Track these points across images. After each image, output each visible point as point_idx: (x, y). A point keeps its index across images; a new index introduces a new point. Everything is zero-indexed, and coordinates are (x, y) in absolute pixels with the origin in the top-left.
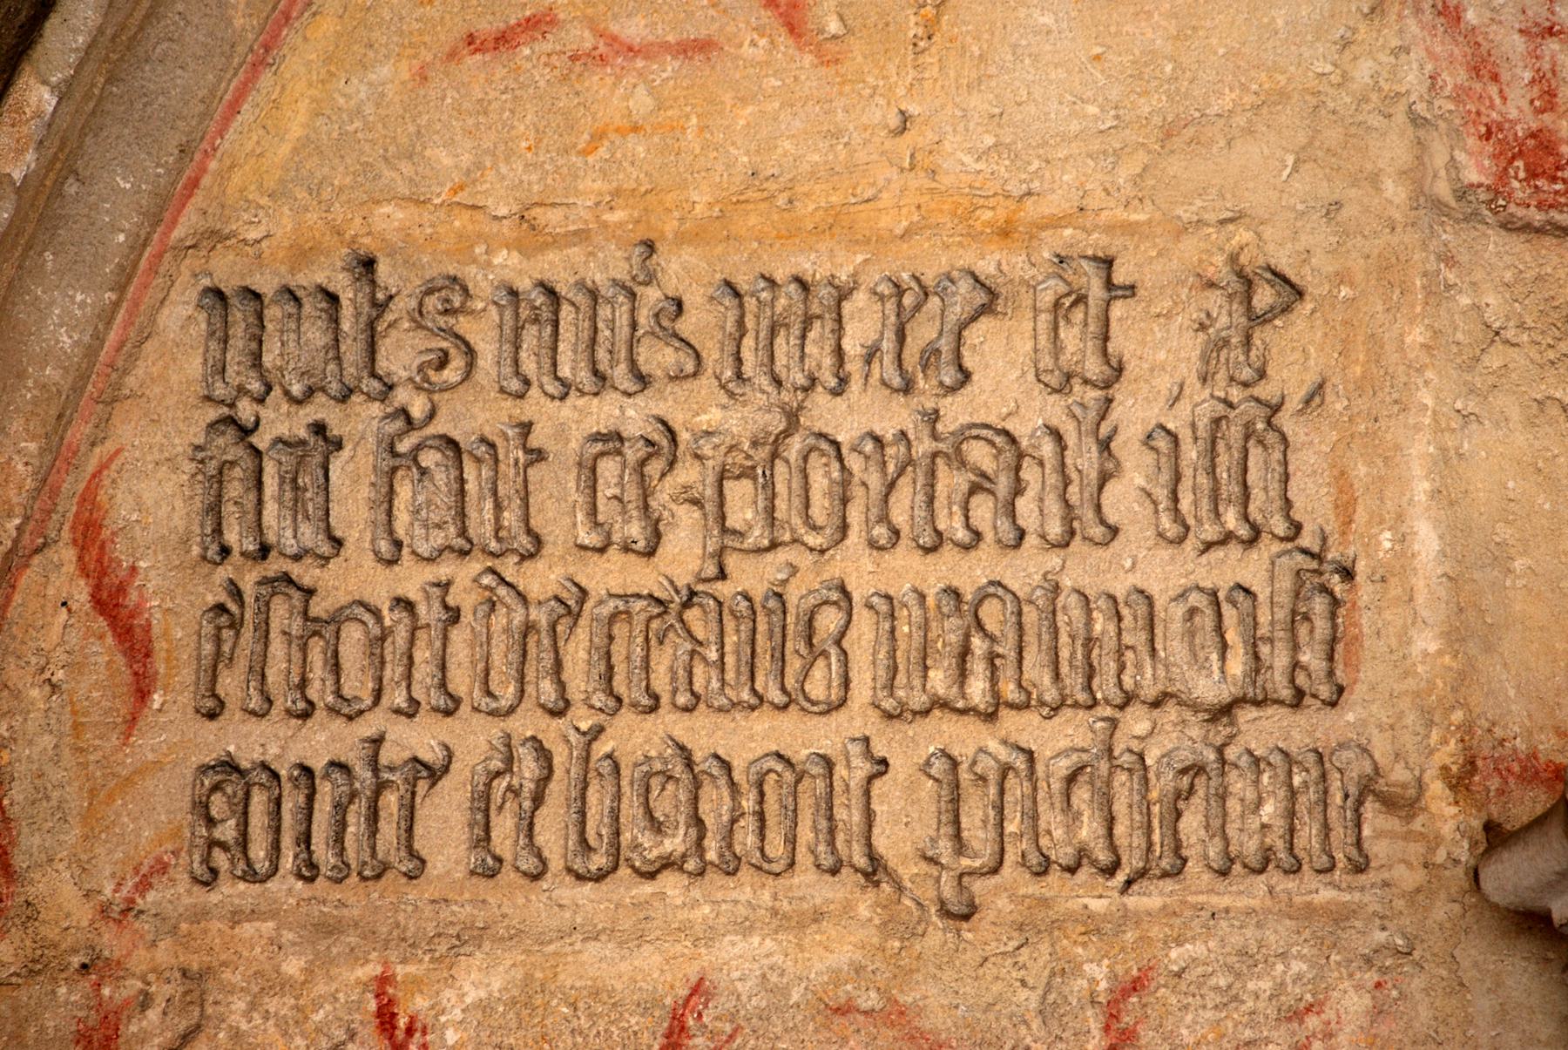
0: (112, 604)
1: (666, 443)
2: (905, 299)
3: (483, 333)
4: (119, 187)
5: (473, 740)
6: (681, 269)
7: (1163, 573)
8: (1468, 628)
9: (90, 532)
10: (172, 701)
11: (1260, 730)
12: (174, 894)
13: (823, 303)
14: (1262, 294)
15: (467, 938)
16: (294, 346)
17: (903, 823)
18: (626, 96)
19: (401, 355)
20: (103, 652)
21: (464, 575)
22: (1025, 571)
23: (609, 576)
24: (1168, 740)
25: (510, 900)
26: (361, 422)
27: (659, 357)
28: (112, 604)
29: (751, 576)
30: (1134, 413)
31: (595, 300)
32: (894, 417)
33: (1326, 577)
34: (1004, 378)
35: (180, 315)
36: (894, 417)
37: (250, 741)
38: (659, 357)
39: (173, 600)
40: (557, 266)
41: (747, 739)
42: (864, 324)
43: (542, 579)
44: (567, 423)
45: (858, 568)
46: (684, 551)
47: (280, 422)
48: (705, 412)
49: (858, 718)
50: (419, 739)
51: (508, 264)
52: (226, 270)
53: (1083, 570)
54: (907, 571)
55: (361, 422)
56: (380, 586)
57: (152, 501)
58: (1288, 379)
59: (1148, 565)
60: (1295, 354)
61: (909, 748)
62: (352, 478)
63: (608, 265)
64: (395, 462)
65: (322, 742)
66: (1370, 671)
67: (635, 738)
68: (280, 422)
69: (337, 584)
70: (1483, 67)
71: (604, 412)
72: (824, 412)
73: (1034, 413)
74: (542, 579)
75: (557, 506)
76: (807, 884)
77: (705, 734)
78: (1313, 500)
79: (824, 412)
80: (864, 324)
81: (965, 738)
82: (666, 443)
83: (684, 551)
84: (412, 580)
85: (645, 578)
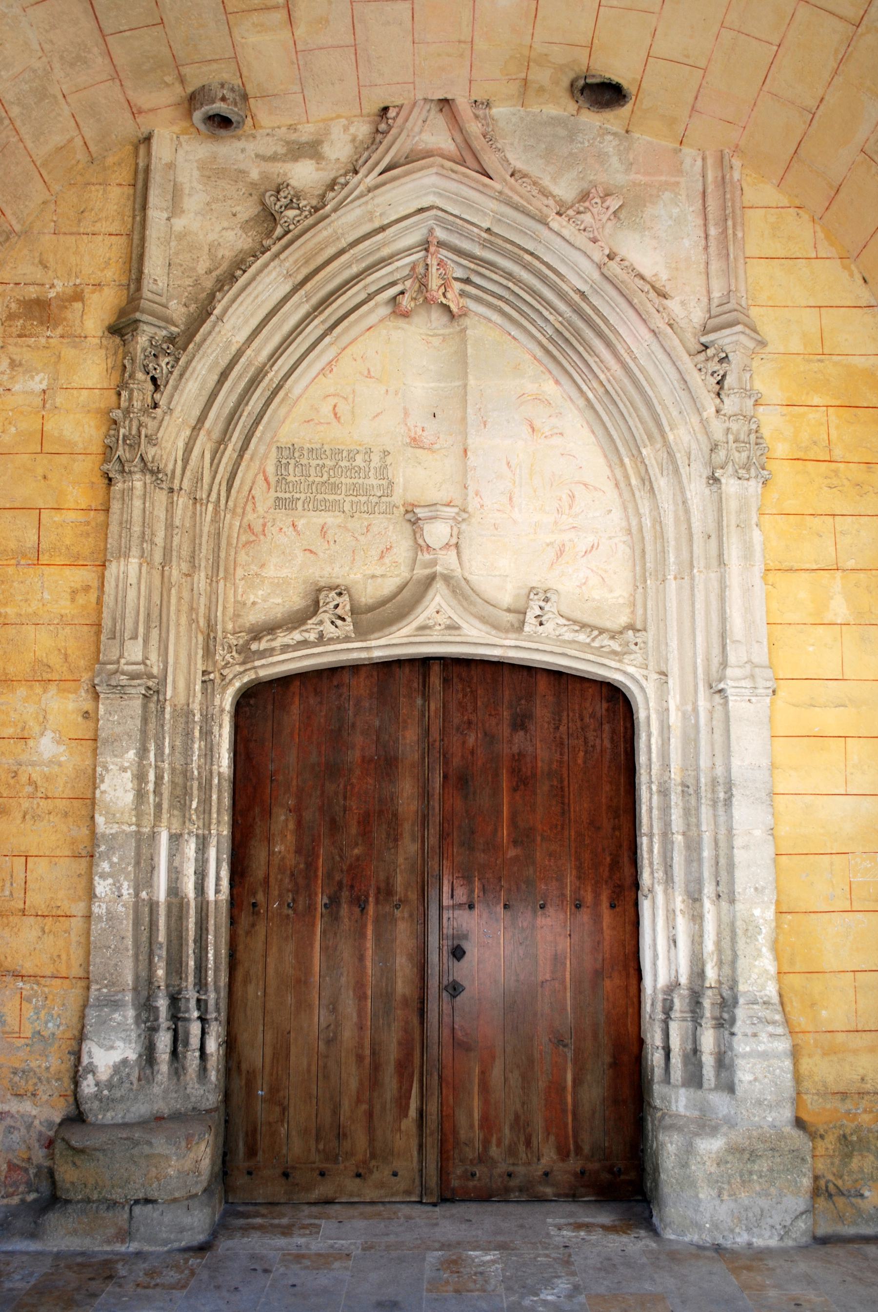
0: (266, 480)
1: (324, 466)
2: (349, 452)
3: (305, 453)
4: (268, 436)
5: (303, 496)
6: (326, 447)
7: (375, 482)
8: (405, 489)
9: (264, 472)
10: (272, 490)
11: (384, 499)
12: (272, 510)
13: (341, 452)
14: (386, 453)
15: (302, 517)
16: (286, 453)
17: (347, 507)
18: (321, 428)
19: (297, 455)
20: (265, 485)
21: (303, 478)
22: (360, 481)
23: (318, 479)
24: (374, 500)
25: (306, 513)
26: (292, 462)
27: (323, 456)
28: (266, 480)
29: (332, 480)
30: (372, 465)
31: (415, 522)
32: (348, 464)
33: (391, 484)
34: (359, 461)
35: (274, 449)
36: (348, 464)
37: (280, 495)
38: (323, 456)
39: (273, 480)
40: (313, 446)
41: (331, 497)
42: (345, 454)
43: (310, 479)
44: (314, 463)
45: (343, 480)
46: (325, 477)
47: (284, 461)
48: (329, 463)
49: (343, 496)
50: (297, 496)
51: (309, 446)
52: (279, 445)
53: (366, 481)
54: (348, 481)
55: (292, 462)
56: (294, 479)
57: (271, 469)
58: (388, 463)
59: (373, 481)
60: (389, 460)
61: (348, 499)
62: (291, 467)
63: (319, 446)
64: (296, 466)
65: (287, 495)
66: (395, 494)
67: (320, 497)
68: (284, 461)
69: (289, 479)
70: (409, 430)
71: (318, 462)
72: (340, 463)
73: (362, 465)
74: (310, 479)
75: (312, 471)
76: (337, 513)
77: (327, 497)
78: (390, 476)
79: (340, 463)
80: (345, 454)
81: (354, 498)
82: (324, 466)
83: (325, 477)
84: (297, 479)
85: (321, 480)
